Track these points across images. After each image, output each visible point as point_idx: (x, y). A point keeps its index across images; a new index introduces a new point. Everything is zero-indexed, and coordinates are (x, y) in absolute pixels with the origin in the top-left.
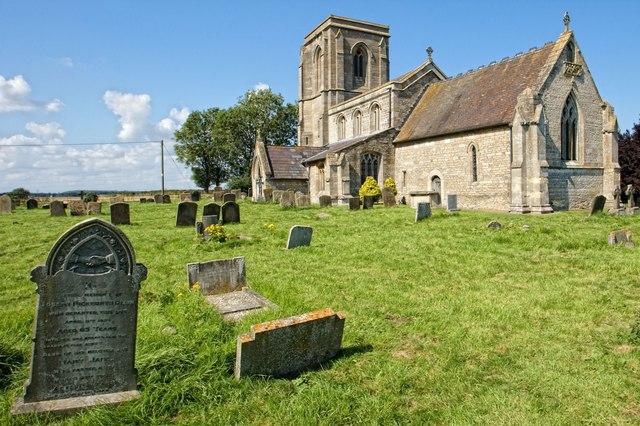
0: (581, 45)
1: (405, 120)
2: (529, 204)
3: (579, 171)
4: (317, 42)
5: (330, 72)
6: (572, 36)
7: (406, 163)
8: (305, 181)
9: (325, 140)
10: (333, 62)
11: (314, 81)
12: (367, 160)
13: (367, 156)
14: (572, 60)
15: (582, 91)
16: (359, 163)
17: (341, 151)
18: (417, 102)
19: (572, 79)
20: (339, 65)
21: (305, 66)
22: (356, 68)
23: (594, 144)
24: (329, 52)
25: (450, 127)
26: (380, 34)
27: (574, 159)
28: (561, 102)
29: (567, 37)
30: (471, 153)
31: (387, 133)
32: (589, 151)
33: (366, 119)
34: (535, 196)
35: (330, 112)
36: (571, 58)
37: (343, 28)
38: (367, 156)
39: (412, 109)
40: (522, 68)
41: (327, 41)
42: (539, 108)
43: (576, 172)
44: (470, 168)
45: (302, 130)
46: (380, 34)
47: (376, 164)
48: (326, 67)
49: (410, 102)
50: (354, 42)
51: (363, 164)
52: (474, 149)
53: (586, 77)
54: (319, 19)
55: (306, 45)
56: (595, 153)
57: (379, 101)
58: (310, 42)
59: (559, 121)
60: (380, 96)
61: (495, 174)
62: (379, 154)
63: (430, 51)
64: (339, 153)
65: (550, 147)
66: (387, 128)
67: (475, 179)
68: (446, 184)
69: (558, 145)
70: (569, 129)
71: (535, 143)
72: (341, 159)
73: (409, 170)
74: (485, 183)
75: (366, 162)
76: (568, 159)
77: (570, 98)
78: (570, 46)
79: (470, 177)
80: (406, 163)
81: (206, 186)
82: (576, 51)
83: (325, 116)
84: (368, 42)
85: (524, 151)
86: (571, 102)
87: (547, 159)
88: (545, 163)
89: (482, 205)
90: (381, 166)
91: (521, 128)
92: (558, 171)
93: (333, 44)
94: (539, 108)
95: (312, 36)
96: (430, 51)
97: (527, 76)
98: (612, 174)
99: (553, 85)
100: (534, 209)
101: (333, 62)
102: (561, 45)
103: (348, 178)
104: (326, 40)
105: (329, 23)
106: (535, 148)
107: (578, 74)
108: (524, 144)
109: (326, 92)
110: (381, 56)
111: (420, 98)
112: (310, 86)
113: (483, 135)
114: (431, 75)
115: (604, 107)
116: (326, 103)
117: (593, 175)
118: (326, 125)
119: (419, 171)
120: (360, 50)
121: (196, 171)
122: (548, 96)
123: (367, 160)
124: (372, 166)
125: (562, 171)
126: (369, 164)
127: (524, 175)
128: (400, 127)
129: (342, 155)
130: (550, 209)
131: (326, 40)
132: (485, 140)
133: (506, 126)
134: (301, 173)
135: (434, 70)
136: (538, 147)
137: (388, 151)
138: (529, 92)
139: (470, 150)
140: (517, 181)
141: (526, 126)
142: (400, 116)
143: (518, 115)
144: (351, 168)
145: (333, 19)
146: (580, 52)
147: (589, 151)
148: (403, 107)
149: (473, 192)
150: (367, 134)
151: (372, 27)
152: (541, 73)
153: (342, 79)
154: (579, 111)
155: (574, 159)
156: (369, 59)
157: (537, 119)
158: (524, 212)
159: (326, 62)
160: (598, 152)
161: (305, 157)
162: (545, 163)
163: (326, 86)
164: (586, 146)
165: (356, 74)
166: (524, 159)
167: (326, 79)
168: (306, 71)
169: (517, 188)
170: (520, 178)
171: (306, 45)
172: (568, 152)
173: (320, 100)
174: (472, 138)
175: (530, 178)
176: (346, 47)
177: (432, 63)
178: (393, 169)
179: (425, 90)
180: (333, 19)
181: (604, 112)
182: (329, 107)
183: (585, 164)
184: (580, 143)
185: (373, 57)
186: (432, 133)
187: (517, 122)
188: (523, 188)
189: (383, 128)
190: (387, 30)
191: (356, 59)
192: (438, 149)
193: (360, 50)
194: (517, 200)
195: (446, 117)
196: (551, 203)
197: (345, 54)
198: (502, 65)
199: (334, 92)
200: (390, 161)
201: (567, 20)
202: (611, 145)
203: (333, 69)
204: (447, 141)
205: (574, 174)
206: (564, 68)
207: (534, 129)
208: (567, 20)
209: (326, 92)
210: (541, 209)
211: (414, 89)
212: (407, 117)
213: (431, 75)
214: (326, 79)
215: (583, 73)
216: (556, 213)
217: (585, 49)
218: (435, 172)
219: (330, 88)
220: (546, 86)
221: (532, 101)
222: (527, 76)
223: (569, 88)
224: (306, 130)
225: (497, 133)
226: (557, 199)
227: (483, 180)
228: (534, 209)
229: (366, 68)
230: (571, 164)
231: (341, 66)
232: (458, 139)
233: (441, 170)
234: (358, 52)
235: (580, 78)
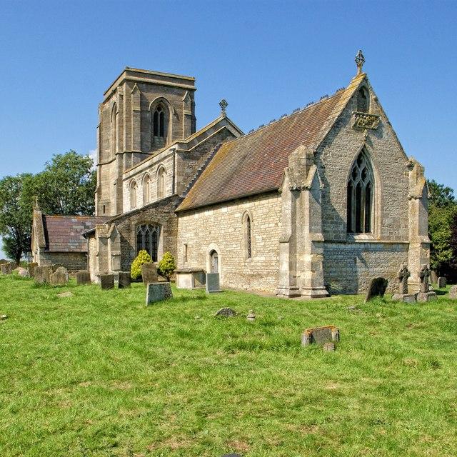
0: (376, 90)
1: (191, 185)
2: (299, 285)
3: (373, 246)
4: (115, 99)
5: (124, 132)
6: (365, 79)
7: (188, 235)
8: (84, 255)
9: (119, 207)
10: (128, 121)
11: (112, 142)
12: (146, 232)
13: (143, 227)
14: (365, 109)
15: (378, 148)
16: (133, 234)
17: (112, 222)
18: (207, 163)
19: (365, 133)
20: (135, 124)
21: (103, 125)
22: (155, 126)
23: (395, 213)
24: (124, 109)
25: (228, 194)
26: (186, 88)
27: (368, 231)
28: (347, 161)
29: (357, 82)
30: (246, 224)
31: (169, 199)
32: (387, 221)
33: (153, 184)
34: (306, 276)
35: (124, 177)
36: (363, 107)
37: (140, 82)
38: (143, 227)
39: (200, 172)
40: (309, 122)
41: (128, 101)
42: (313, 169)
43: (368, 247)
44: (244, 242)
45: (99, 198)
46: (186, 88)
47: (155, 236)
48: (121, 127)
49: (198, 165)
50: (152, 97)
51: (139, 236)
52: (249, 220)
53: (385, 131)
54: (112, 73)
55: (104, 103)
56: (395, 225)
57: (166, 164)
58: (108, 99)
59: (345, 185)
60: (166, 157)
61: (253, 249)
62: (158, 225)
63: (223, 104)
64: (110, 223)
65: (327, 217)
66: (171, 194)
67: (250, 255)
68: (223, 259)
69: (343, 214)
70: (359, 196)
71: (307, 212)
72: (111, 229)
73: (190, 243)
74: (259, 259)
75: (143, 233)
76: (359, 231)
77: (362, 157)
78: (362, 92)
79: (245, 252)
80: (188, 235)
81: (18, 257)
82: (372, 97)
83: (119, 183)
84: (169, 97)
85: (293, 222)
86: (364, 160)
87: (324, 232)
88: (319, 236)
89: (257, 286)
90: (161, 238)
91: (290, 194)
92: (342, 246)
93: (128, 101)
94: (313, 169)
95: (110, 92)
96: (223, 104)
97: (311, 131)
98: (418, 250)
99: (337, 141)
100: (305, 292)
101: (128, 121)
102: (351, 91)
103: (119, 252)
104: (121, 96)
105: (124, 76)
106: (307, 218)
107: (373, 126)
108: (294, 213)
109: (121, 155)
110: (185, 112)
111: (210, 159)
112: (108, 148)
113: (257, 203)
114: (225, 132)
115: (411, 167)
116: (120, 167)
117: (393, 251)
118: (120, 192)
119: (199, 245)
120: (161, 106)
121: (7, 241)
122: (328, 156)
123: (146, 232)
124: (151, 239)
125: (349, 247)
126: (147, 236)
127: (292, 251)
128: (185, 194)
129: (113, 225)
130: (326, 292)
131: (121, 96)
132: (258, 208)
133: (274, 192)
134: (80, 246)
135: (229, 128)
136: (310, 217)
137: (170, 221)
138: (301, 151)
139: (245, 219)
140: (285, 257)
141: (296, 192)
142: (185, 180)
143: (287, 179)
144: (123, 240)
145: (129, 72)
146: (376, 100)
147: (387, 221)
148: (189, 171)
149: (248, 271)
150: (139, 205)
151: (174, 79)
152: (323, 128)
153: (138, 139)
154: (375, 173)
155: (368, 231)
156: (171, 115)
157: (309, 183)
158: (291, 296)
159: (121, 121)
160: (402, 226)
161: (88, 228)
162: (319, 236)
163: (121, 148)
164: (384, 216)
165: (155, 134)
166: (294, 231)
167: (121, 140)
168: (103, 132)
169: (285, 267)
170: (288, 255)
171: (104, 103)
172: (358, 216)
173: (115, 164)
174: (247, 205)
175: (300, 255)
176: (143, 103)
177: (226, 119)
178: (176, 242)
179: (216, 151)
180: (129, 72)
181: (410, 173)
182: (124, 171)
183: (382, 238)
184: (376, 213)
185: (175, 114)
186: (211, 200)
187: (286, 187)
188: (292, 266)
189: (167, 194)
190: (192, 82)
191: (155, 113)
192: (216, 219)
193: (161, 106)
194: (285, 281)
195: (228, 181)
196: (327, 288)
197: (141, 111)
198: (292, 118)
199: (129, 154)
200: (171, 232)
201: (360, 60)
202: (417, 213)
203: (128, 128)
204: (224, 210)
205: (367, 250)
206: (353, 120)
207: (306, 194)
208: (360, 60)
209: (121, 155)
210: (310, 293)
211: (202, 150)
212: (194, 181)
213: (225, 132)
214: (121, 140)
215: (380, 125)
216: (333, 297)
217: (384, 97)
218: (213, 247)
219: (124, 150)
220: (326, 142)
221: (304, 161)
222: (311, 131)
223: (360, 145)
224: (103, 197)
225: (270, 200)
226: (335, 279)
227: (256, 256)
228: (305, 292)
229: (167, 128)
230: (363, 237)
231: (138, 125)
232: (234, 208)
233: (218, 243)
234: (159, 109)
235: (377, 131)
